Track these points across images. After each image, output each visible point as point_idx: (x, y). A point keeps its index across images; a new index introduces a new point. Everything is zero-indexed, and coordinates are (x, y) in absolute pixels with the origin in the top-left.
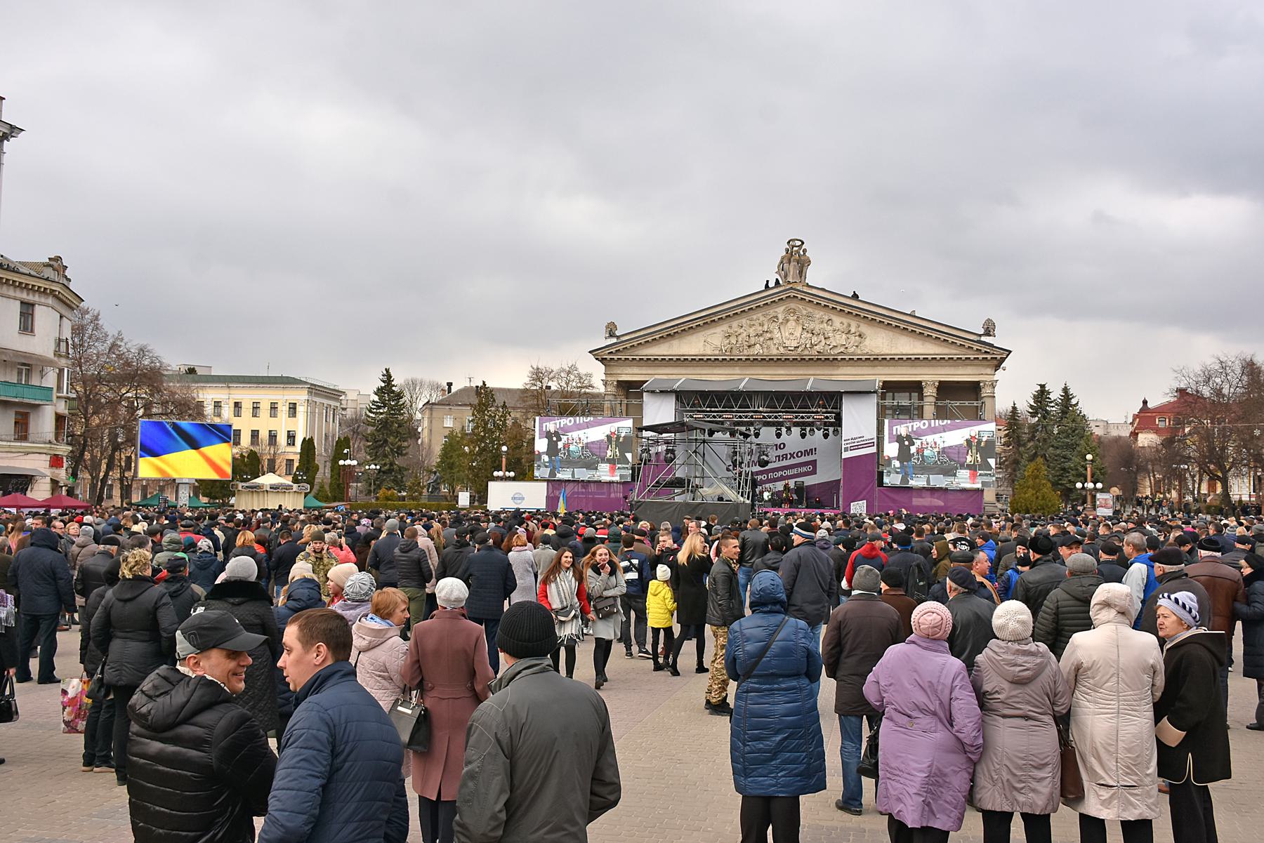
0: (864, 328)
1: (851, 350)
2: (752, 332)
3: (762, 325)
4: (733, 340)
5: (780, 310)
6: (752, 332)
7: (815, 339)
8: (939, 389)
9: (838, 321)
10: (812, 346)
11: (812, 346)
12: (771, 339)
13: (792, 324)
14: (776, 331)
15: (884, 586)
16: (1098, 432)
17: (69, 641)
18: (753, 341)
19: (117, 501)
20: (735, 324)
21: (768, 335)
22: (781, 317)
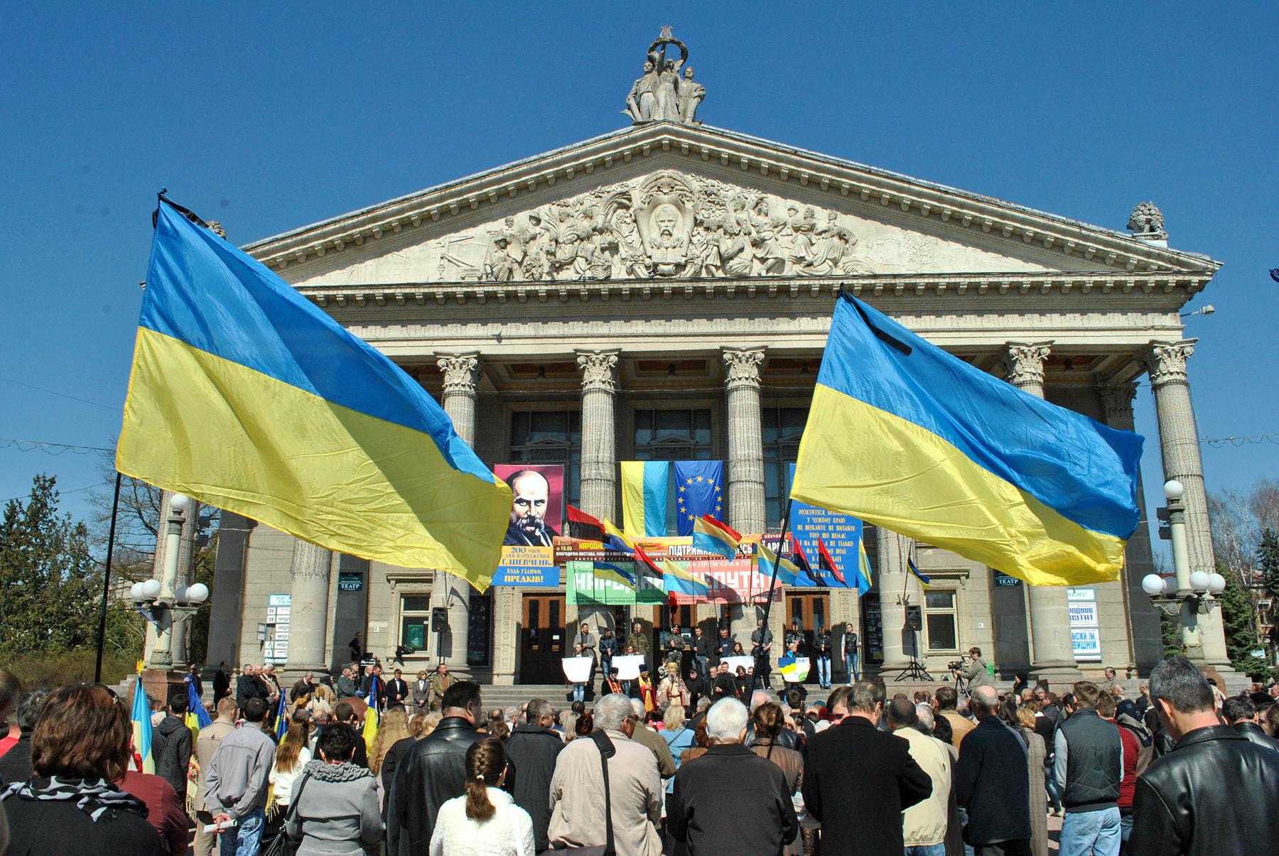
0: (848, 222)
1: (824, 269)
2: (563, 230)
3: (588, 215)
4: (515, 252)
5: (637, 186)
6: (563, 230)
7: (728, 245)
8: (477, 374)
9: (779, 206)
10: (725, 260)
11: (725, 260)
12: (613, 248)
13: (667, 209)
14: (625, 229)
15: (798, 801)
16: (710, 735)
17: (901, 449)
18: (563, 253)
19: (75, 618)
20: (522, 218)
21: (608, 238)
22: (638, 197)
